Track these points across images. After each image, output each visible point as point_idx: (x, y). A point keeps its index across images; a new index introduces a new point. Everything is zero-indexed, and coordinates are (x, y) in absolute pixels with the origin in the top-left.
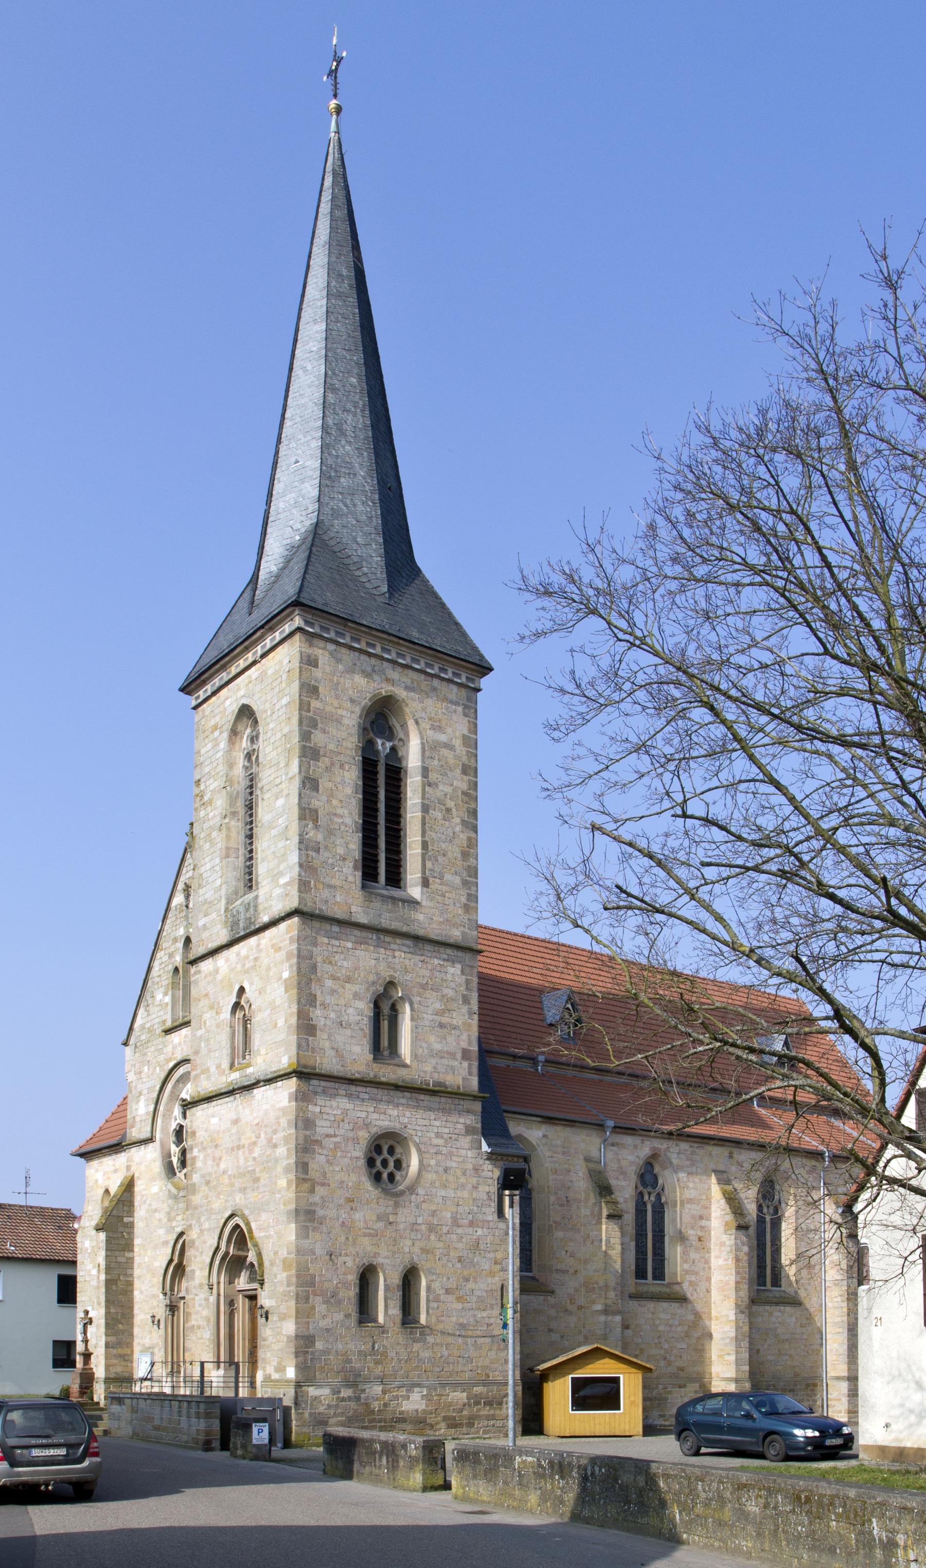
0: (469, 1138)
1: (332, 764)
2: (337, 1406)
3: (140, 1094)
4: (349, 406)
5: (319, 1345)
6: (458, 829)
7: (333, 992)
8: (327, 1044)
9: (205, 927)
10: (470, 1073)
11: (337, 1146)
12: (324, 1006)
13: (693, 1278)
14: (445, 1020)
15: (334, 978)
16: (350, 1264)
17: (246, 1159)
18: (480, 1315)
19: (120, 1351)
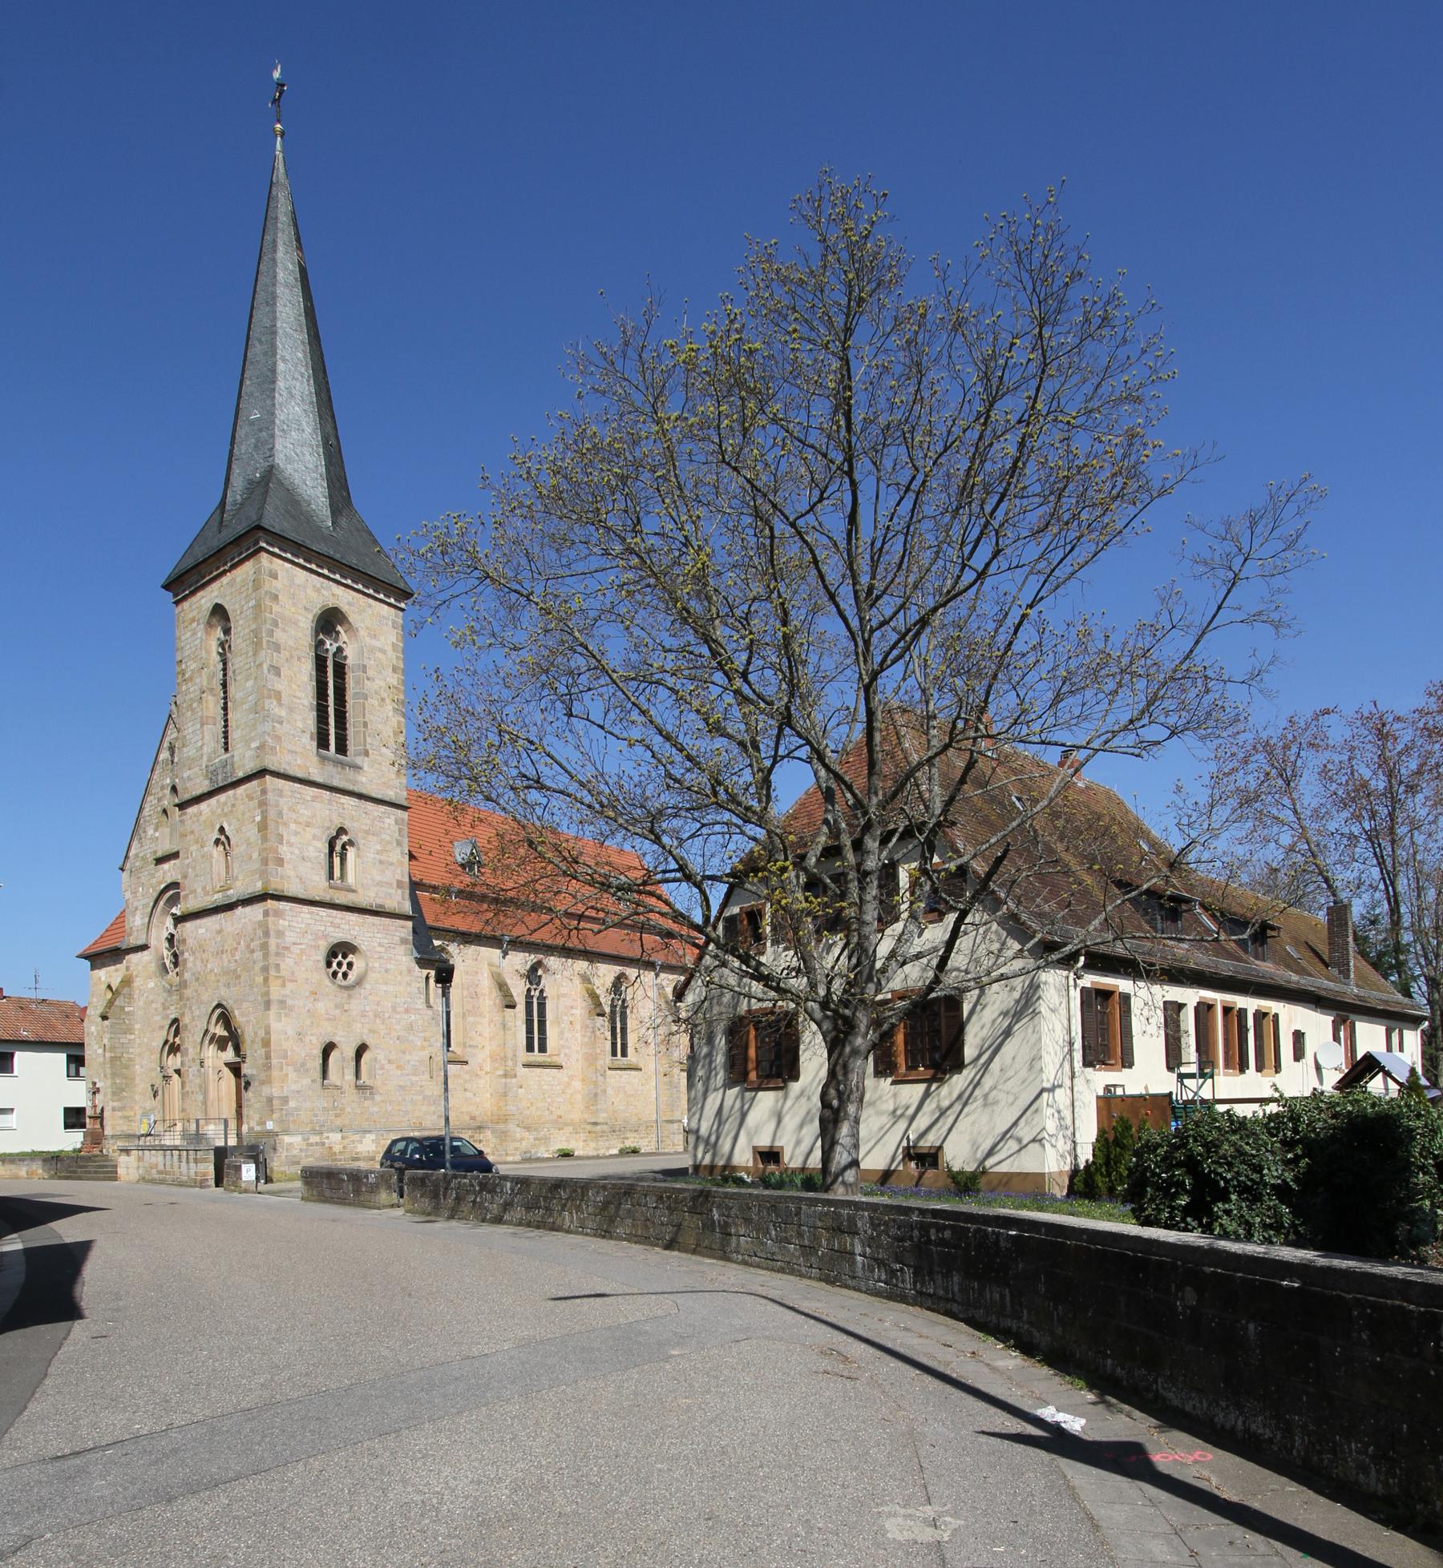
1: (292, 657)
5: (292, 1104)
7: (296, 833)
8: (292, 874)
9: (189, 779)
11: (303, 952)
14: (383, 858)
15: (296, 822)
18: (414, 1078)
19: (125, 1113)
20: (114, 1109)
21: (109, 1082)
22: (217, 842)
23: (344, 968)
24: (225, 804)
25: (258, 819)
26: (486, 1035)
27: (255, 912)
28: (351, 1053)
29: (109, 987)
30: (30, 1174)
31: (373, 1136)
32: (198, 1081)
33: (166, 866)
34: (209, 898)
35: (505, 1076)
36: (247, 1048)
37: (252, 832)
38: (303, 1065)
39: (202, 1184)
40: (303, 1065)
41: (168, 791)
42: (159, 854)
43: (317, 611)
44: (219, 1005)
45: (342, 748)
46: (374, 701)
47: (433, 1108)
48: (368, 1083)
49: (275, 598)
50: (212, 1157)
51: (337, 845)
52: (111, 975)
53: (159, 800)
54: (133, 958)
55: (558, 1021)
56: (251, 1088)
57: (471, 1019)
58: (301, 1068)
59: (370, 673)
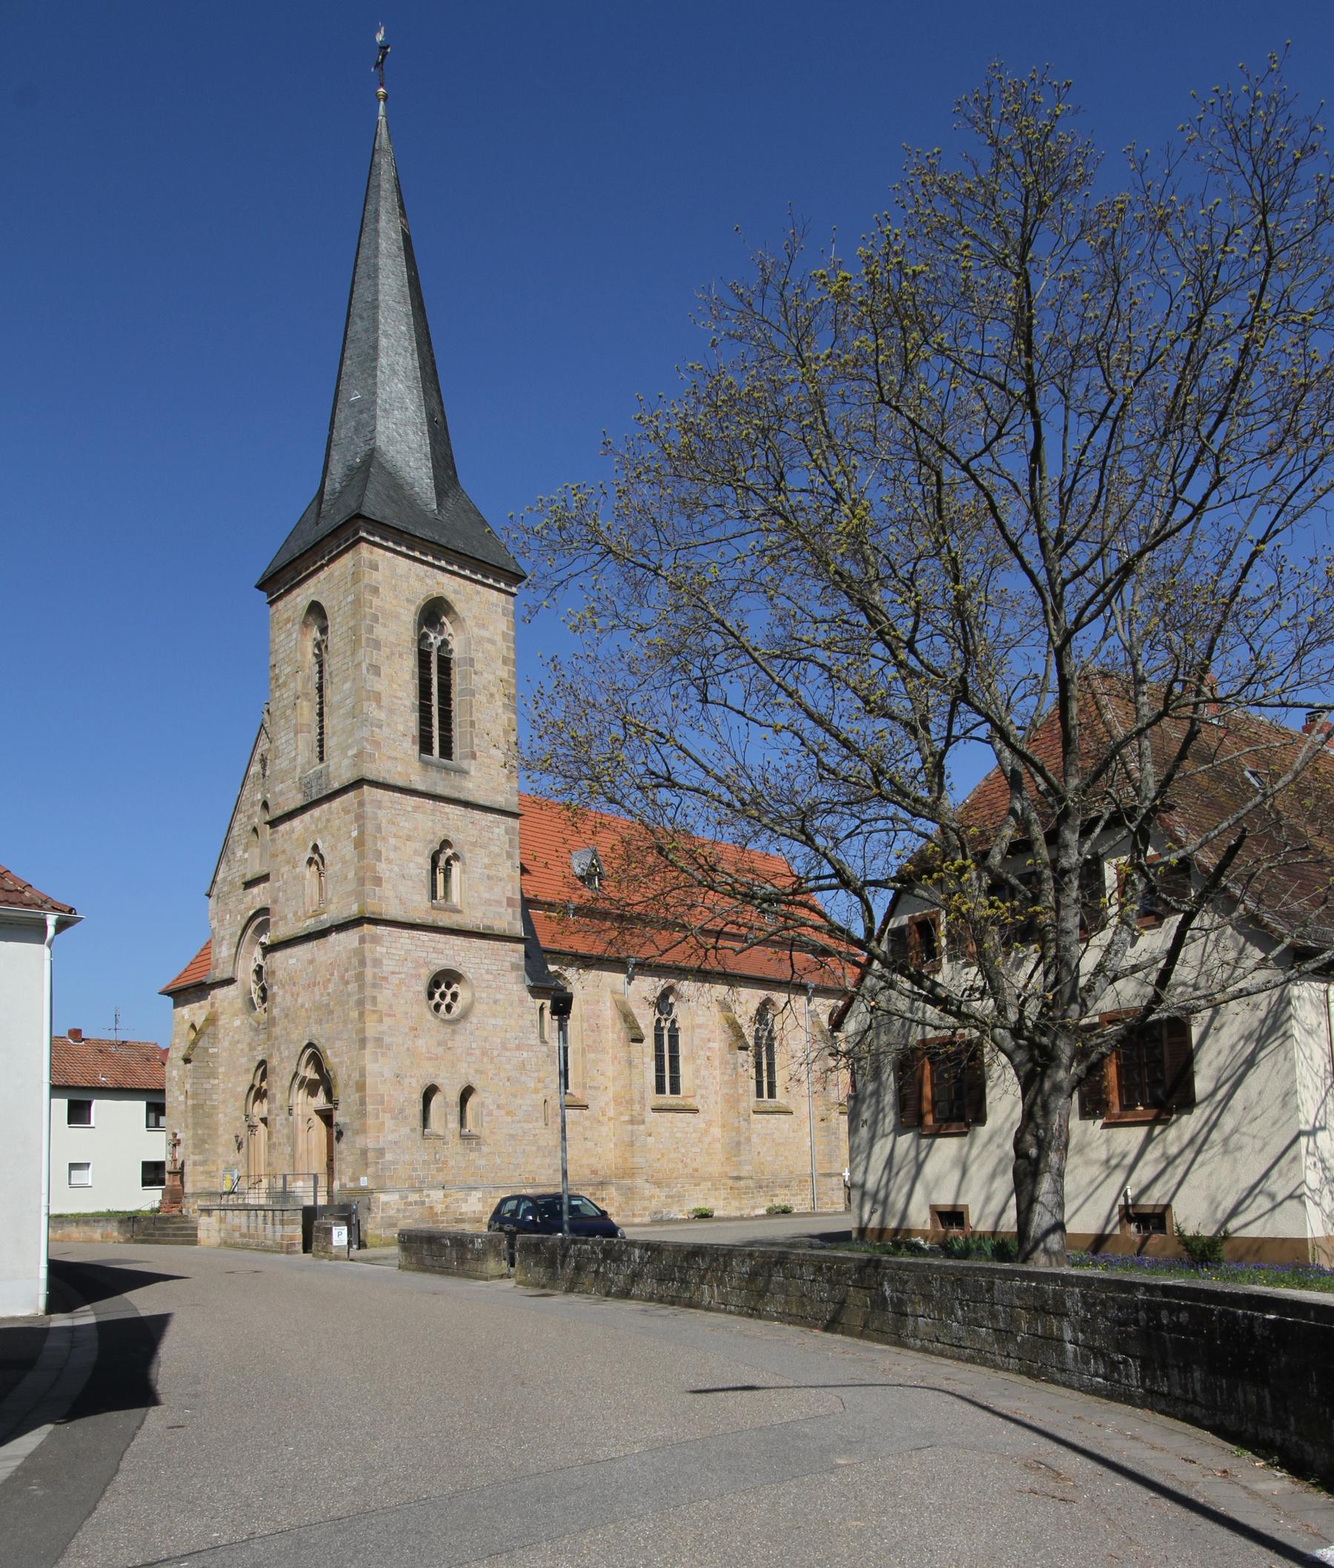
0: (514, 974)
1: (393, 654)
2: (405, 1210)
3: (223, 939)
4: (400, 350)
5: (389, 1157)
6: (500, 710)
7: (396, 849)
8: (390, 894)
10: (514, 918)
11: (402, 982)
12: (389, 861)
13: (704, 1092)
14: (492, 873)
15: (395, 836)
16: (414, 1084)
17: (322, 995)
18: (526, 1126)
19: (206, 1168)
20: (195, 1164)
21: (190, 1133)
22: (310, 861)
23: (448, 999)
24: (319, 819)
25: (355, 834)
26: (609, 1074)
27: (349, 939)
28: (454, 1097)
29: (193, 1026)
30: (105, 1237)
31: (479, 1194)
32: (285, 1131)
33: (255, 890)
34: (300, 924)
35: (632, 1122)
36: (339, 1093)
37: (348, 850)
38: (401, 1111)
39: (289, 1250)
40: (401, 1111)
41: (258, 808)
42: (249, 877)
43: (420, 602)
44: (310, 1045)
45: (446, 751)
46: (481, 698)
47: (548, 1161)
48: (473, 1132)
49: (375, 590)
50: (300, 1218)
51: (441, 860)
52: (194, 1012)
53: (249, 817)
54: (219, 993)
55: (692, 1057)
56: (344, 1139)
57: (591, 1056)
58: (399, 1115)
59: (478, 666)
